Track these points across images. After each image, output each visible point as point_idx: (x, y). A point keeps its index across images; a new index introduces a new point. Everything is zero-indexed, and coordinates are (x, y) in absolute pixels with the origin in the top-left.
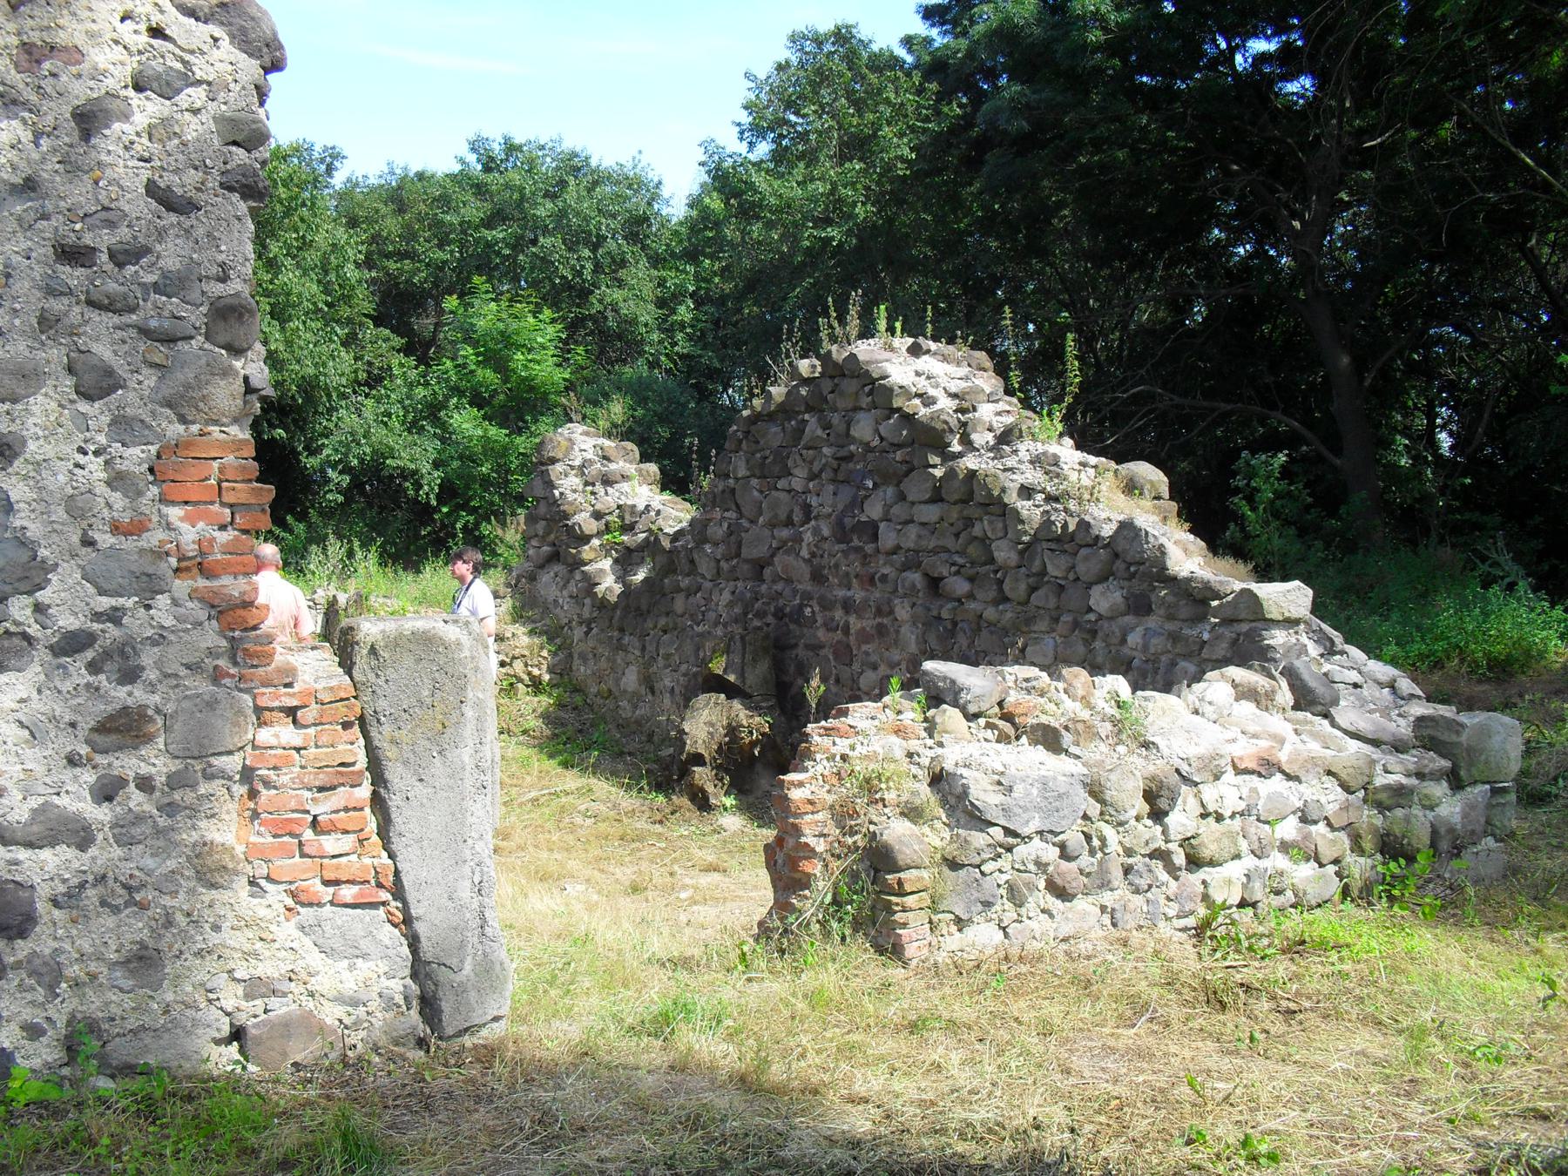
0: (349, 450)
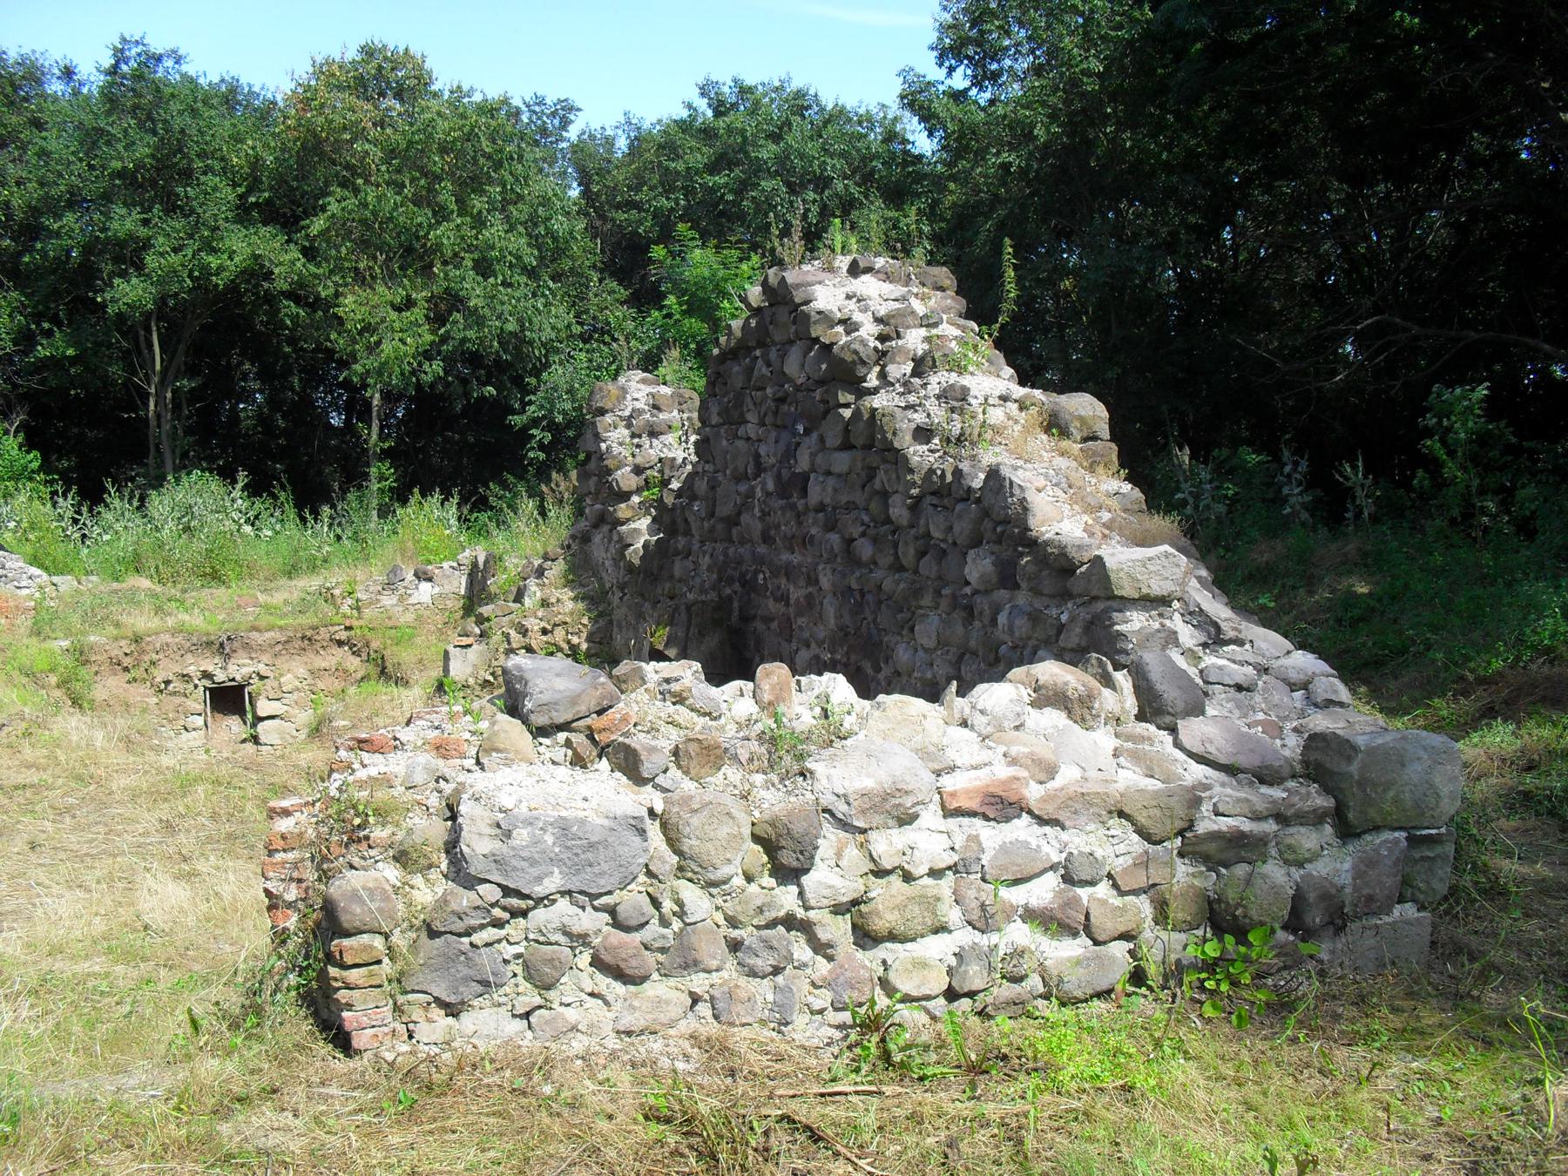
0: (553, 405)
